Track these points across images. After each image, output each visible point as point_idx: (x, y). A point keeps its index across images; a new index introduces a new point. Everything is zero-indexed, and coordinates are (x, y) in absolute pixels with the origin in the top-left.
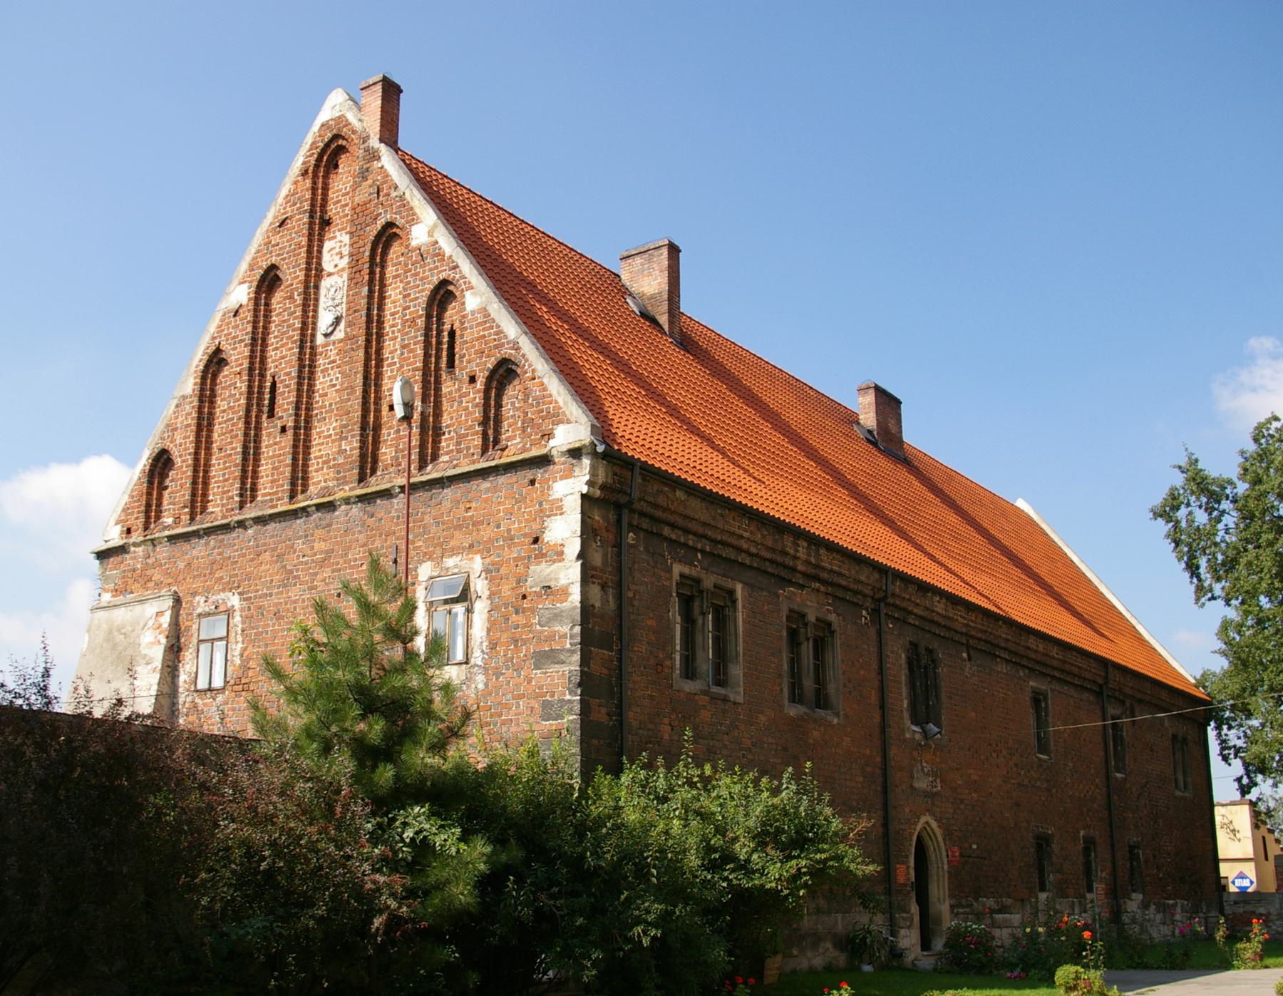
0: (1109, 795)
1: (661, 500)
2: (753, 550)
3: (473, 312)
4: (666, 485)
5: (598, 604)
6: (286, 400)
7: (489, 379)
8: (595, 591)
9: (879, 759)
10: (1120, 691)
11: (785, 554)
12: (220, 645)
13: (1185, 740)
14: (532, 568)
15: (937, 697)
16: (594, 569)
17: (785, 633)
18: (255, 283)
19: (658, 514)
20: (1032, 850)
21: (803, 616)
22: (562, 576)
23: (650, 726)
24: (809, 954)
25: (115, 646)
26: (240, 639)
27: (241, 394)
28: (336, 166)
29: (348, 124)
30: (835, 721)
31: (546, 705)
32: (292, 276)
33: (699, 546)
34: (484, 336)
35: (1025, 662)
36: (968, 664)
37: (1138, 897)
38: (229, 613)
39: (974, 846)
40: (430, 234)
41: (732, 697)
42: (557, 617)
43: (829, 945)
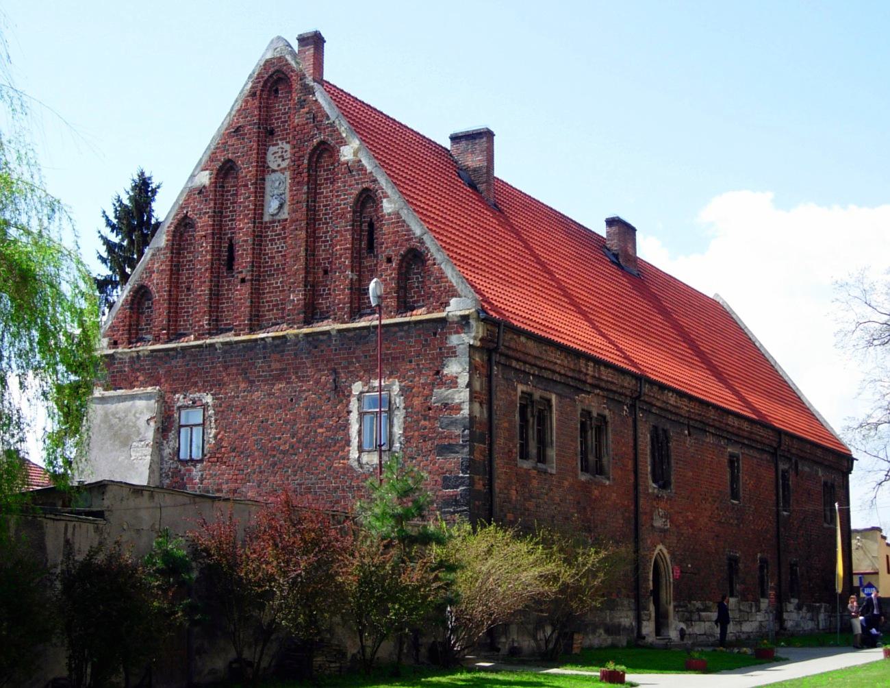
0: (778, 528)
1: (512, 344)
2: (563, 372)
3: (389, 214)
4: (515, 334)
5: (478, 415)
6: (244, 259)
7: (401, 261)
8: (477, 406)
9: (632, 507)
10: (789, 451)
11: (580, 372)
12: (197, 432)
13: (833, 486)
14: (435, 390)
15: (669, 463)
16: (476, 392)
17: (579, 426)
18: (215, 172)
19: (511, 353)
20: (726, 568)
21: (589, 413)
22: (456, 397)
23: (506, 491)
24: (591, 637)
25: (111, 427)
26: (213, 425)
27: (207, 252)
28: (276, 91)
29: (288, 64)
30: (608, 483)
31: (445, 479)
32: (247, 170)
33: (532, 372)
34: (398, 231)
35: (725, 434)
36: (688, 438)
37: (795, 601)
38: (205, 407)
39: (689, 566)
40: (355, 154)
41: (549, 470)
42: (454, 423)
43: (602, 631)
